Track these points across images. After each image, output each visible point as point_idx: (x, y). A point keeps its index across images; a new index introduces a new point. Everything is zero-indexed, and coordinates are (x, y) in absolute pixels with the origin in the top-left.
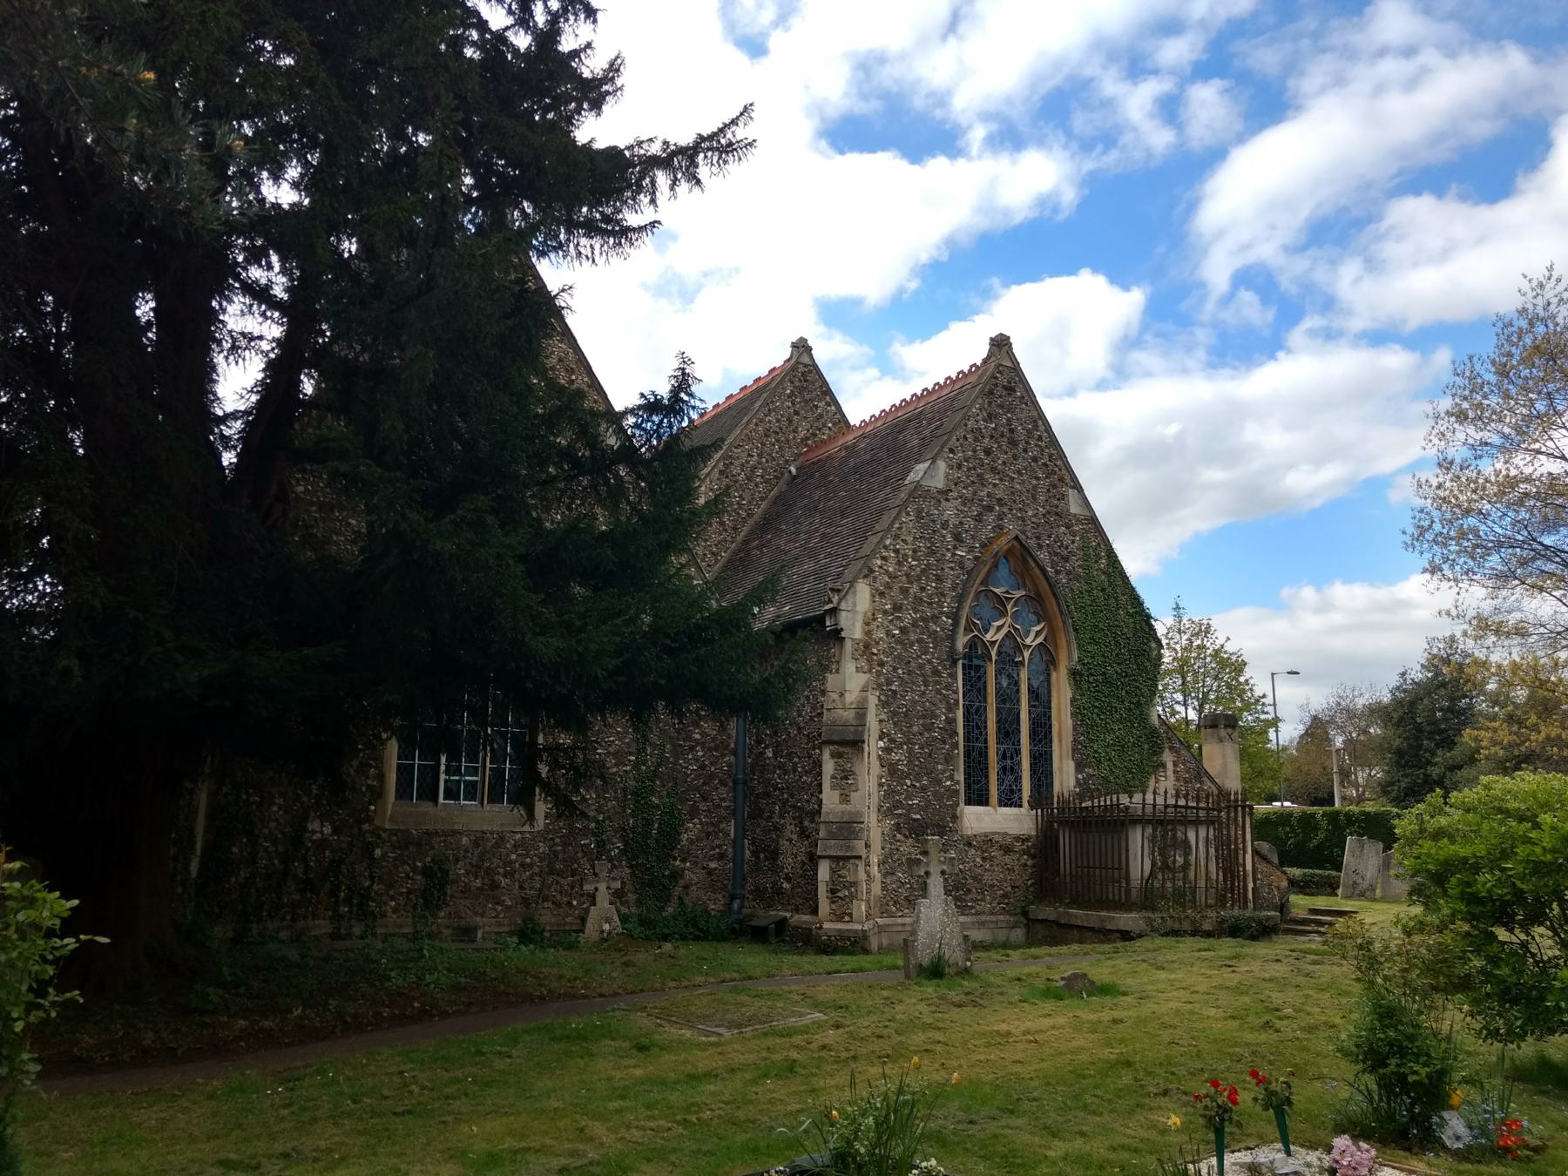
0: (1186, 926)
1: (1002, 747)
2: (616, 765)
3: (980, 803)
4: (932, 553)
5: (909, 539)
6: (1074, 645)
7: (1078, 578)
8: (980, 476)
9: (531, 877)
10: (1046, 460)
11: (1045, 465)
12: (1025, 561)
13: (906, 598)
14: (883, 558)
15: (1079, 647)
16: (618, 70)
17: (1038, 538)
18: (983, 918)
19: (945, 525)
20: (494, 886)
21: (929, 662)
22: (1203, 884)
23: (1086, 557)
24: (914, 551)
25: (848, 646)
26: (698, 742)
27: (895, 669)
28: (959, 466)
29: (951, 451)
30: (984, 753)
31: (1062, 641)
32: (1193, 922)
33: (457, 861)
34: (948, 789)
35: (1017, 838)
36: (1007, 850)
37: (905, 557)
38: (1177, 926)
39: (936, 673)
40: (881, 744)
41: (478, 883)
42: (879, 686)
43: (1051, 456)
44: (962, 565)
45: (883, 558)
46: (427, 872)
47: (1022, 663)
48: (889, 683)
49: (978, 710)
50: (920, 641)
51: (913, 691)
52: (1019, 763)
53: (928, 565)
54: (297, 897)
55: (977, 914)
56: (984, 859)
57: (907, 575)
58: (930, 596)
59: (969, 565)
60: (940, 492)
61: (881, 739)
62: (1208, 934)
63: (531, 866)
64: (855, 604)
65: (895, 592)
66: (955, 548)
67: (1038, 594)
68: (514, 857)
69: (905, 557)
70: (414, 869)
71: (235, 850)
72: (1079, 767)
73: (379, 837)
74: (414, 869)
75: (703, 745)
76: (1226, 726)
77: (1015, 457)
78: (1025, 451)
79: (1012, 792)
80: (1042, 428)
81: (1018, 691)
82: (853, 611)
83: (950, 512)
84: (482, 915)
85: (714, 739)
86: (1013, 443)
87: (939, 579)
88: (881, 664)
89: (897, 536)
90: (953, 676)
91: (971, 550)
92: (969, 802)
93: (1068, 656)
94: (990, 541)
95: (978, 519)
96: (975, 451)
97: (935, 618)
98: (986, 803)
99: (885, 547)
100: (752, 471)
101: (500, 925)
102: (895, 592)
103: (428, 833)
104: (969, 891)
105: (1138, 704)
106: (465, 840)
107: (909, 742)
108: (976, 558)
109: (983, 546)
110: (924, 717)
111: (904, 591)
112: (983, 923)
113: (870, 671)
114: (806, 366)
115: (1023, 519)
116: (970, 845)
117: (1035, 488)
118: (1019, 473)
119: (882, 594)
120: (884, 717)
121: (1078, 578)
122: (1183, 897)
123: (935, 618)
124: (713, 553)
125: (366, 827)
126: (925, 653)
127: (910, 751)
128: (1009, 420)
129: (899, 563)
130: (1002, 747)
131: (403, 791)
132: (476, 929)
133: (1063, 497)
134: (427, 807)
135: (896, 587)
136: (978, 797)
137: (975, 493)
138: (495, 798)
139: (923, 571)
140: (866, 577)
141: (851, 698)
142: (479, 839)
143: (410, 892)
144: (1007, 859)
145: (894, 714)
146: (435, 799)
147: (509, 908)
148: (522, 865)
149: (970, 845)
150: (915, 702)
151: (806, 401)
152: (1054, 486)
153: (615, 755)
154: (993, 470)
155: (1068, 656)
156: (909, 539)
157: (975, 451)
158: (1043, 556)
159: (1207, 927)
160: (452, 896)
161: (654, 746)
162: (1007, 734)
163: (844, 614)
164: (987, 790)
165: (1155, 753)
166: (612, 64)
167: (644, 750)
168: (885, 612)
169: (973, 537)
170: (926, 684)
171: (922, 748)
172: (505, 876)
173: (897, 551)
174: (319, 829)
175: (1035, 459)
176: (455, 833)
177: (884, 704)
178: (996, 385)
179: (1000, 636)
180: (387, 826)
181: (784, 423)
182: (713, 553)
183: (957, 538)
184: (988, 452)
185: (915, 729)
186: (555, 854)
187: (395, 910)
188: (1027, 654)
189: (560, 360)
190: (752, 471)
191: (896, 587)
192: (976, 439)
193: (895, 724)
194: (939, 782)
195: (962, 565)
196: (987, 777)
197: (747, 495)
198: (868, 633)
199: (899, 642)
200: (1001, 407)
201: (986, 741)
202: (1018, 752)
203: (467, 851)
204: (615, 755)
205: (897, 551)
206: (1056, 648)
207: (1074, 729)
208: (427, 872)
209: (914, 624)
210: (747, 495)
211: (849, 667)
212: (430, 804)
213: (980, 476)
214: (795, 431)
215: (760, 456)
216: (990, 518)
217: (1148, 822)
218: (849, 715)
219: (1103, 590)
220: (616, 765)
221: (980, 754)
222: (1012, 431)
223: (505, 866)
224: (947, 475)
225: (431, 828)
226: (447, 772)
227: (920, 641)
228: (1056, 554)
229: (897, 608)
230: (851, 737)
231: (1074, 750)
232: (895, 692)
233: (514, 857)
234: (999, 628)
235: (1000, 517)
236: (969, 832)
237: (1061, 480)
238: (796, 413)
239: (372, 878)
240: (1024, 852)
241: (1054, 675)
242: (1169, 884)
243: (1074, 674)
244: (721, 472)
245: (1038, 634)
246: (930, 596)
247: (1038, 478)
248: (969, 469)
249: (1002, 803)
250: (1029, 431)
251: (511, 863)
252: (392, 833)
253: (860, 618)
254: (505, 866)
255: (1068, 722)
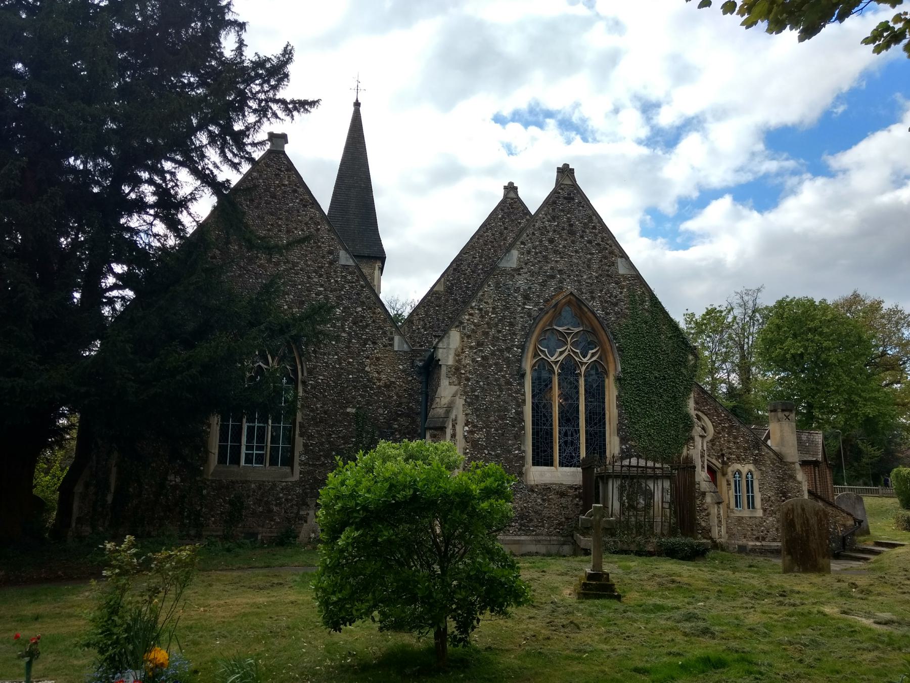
0: (633, 547)
1: (564, 429)
2: (344, 444)
3: (546, 465)
4: (507, 308)
5: (490, 301)
6: (618, 359)
7: (625, 316)
8: (545, 257)
9: (292, 506)
10: (599, 241)
11: (598, 244)
12: (581, 309)
13: (487, 338)
14: (471, 314)
15: (623, 362)
16: (291, 53)
17: (592, 292)
18: (540, 538)
19: (517, 290)
20: (270, 511)
21: (503, 376)
22: (659, 519)
23: (633, 302)
24: (493, 308)
25: (444, 370)
26: (396, 430)
27: (478, 382)
28: (529, 252)
29: (523, 243)
30: (550, 433)
31: (611, 359)
32: (639, 544)
33: (249, 497)
34: (516, 455)
35: (571, 487)
36: (562, 494)
37: (487, 313)
38: (625, 547)
39: (508, 383)
40: (467, 428)
41: (261, 509)
42: (466, 393)
43: (603, 238)
44: (529, 315)
45: (471, 314)
46: (231, 503)
47: (580, 374)
48: (473, 390)
49: (544, 406)
50: (496, 364)
51: (491, 395)
52: (579, 439)
53: (504, 317)
54: (162, 514)
55: (536, 535)
56: (544, 500)
57: (488, 323)
58: (504, 336)
59: (535, 314)
60: (514, 270)
61: (466, 425)
62: (650, 554)
63: (291, 500)
64: (448, 344)
65: (479, 335)
66: (524, 304)
67: (593, 329)
68: (281, 495)
69: (487, 313)
70: (225, 501)
71: (131, 490)
72: (623, 440)
73: (205, 483)
74: (225, 501)
75: (400, 432)
76: (783, 411)
77: (573, 242)
78: (582, 237)
79: (572, 457)
80: (596, 221)
81: (578, 392)
82: (448, 348)
83: (521, 282)
84: (263, 526)
85: (407, 428)
86: (572, 233)
87: (512, 325)
88: (468, 379)
89: (481, 300)
90: (522, 385)
91: (537, 304)
92: (534, 464)
93: (615, 368)
94: (552, 297)
95: (543, 284)
96: (541, 241)
97: (509, 349)
98: (552, 465)
99: (472, 308)
100: (476, 267)
101: (272, 532)
102: (479, 335)
103: (232, 482)
104: (531, 520)
105: (675, 398)
106: (253, 486)
107: (487, 426)
108: (541, 309)
109: (546, 301)
110: (499, 411)
111: (486, 334)
112: (539, 541)
113: (459, 384)
114: (512, 199)
115: (579, 282)
116: (533, 491)
117: (590, 260)
118: (576, 252)
119: (469, 337)
120: (469, 411)
121: (625, 316)
122: (644, 528)
123: (509, 349)
124: (449, 318)
125: (198, 478)
126: (500, 371)
127: (488, 433)
128: (568, 218)
129: (482, 317)
130: (564, 429)
131: (222, 459)
132: (257, 534)
133: (613, 264)
134: (234, 468)
135: (479, 332)
136: (542, 458)
137: (541, 268)
138: (273, 462)
139: (500, 320)
140: (457, 327)
141: (445, 401)
142: (261, 485)
143: (222, 513)
144: (563, 500)
145: (477, 410)
146: (238, 463)
147: (278, 523)
148: (286, 500)
149: (533, 491)
150: (492, 402)
151: (513, 221)
152: (606, 258)
153: (343, 438)
154: (556, 252)
155: (615, 368)
156: (490, 301)
157: (541, 241)
158: (595, 305)
159: (650, 548)
160: (246, 516)
161: (368, 432)
162: (568, 420)
163: (440, 350)
164: (552, 456)
165: (687, 431)
166: (285, 49)
167: (361, 435)
168: (471, 348)
169: (538, 296)
170: (501, 390)
171: (496, 430)
172: (276, 506)
173: (480, 310)
174: (174, 479)
175: (590, 242)
176: (246, 482)
177: (468, 404)
178: (559, 197)
179: (561, 358)
180: (210, 478)
181: (497, 235)
182: (449, 318)
183: (526, 298)
184: (551, 241)
185: (492, 418)
186: (306, 494)
187: (214, 523)
188: (583, 369)
189: (311, 218)
190: (476, 267)
191: (479, 332)
192: (542, 234)
193: (477, 416)
194: (510, 452)
195: (529, 315)
196: (552, 448)
197: (472, 281)
198: (459, 361)
199: (481, 365)
200: (563, 211)
201: (551, 425)
202: (577, 432)
203: (254, 492)
204: (343, 438)
205: (480, 310)
206: (607, 363)
207: (619, 415)
208: (231, 503)
209: (493, 353)
210: (472, 281)
211: (444, 382)
212: (236, 466)
213: (545, 257)
214: (505, 239)
215: (481, 257)
216: (553, 283)
217: (617, 477)
218: (441, 411)
219: (646, 323)
220: (344, 444)
221: (547, 433)
222: (571, 225)
223: (276, 500)
224: (519, 258)
225: (233, 479)
226: (248, 448)
227: (496, 364)
228: (606, 302)
229: (480, 344)
230: (439, 425)
231: (619, 430)
232: (477, 396)
233: (281, 495)
234: (561, 353)
235: (561, 282)
236: (533, 483)
237: (612, 253)
238: (506, 228)
239: (201, 505)
240: (576, 496)
241: (607, 381)
242: (633, 519)
243: (618, 379)
244: (455, 270)
245: (593, 355)
246: (504, 336)
247: (593, 254)
248: (536, 253)
249: (562, 464)
250: (585, 224)
251: (280, 498)
252: (213, 481)
253: (452, 353)
254: (276, 500)
255: (615, 411)
